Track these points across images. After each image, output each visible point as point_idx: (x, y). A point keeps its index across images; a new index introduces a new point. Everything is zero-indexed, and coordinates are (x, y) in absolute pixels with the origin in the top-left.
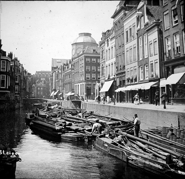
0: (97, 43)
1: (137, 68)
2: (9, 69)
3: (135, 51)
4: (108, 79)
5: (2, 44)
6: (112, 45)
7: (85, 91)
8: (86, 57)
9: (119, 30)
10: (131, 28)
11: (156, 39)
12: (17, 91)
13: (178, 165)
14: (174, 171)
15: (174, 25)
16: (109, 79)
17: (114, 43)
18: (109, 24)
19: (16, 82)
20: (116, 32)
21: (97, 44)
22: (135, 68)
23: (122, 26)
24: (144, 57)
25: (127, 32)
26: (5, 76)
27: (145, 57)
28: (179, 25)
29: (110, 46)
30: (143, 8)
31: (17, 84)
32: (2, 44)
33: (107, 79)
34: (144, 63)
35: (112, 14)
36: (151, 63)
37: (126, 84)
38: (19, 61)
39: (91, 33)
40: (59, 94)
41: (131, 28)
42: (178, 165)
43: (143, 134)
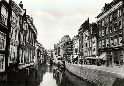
16: (76, 54)
18: (77, 33)
20: (79, 37)
32: (92, 23)
33: (75, 54)
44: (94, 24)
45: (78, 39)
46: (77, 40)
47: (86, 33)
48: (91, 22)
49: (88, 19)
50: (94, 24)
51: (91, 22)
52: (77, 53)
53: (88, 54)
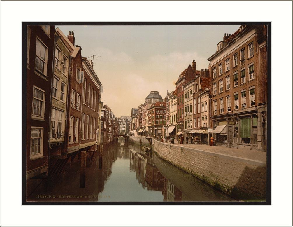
1: (192, 119)
3: (102, 124)
4: (172, 125)
6: (175, 102)
8: (156, 109)
10: (186, 94)
12: (110, 131)
14: (239, 200)
15: (235, 86)
16: (172, 125)
18: (173, 88)
19: (110, 125)
20: (177, 94)
22: (191, 119)
23: (183, 90)
25: (186, 94)
26: (80, 69)
29: (173, 103)
31: (110, 126)
34: (197, 116)
35: (176, 81)
37: (184, 129)
38: (110, 110)
39: (132, 109)
41: (186, 94)
44: (204, 71)
45: (174, 99)
46: (173, 101)
47: (191, 88)
49: (194, 62)
50: (204, 71)
52: (174, 124)
53: (195, 126)
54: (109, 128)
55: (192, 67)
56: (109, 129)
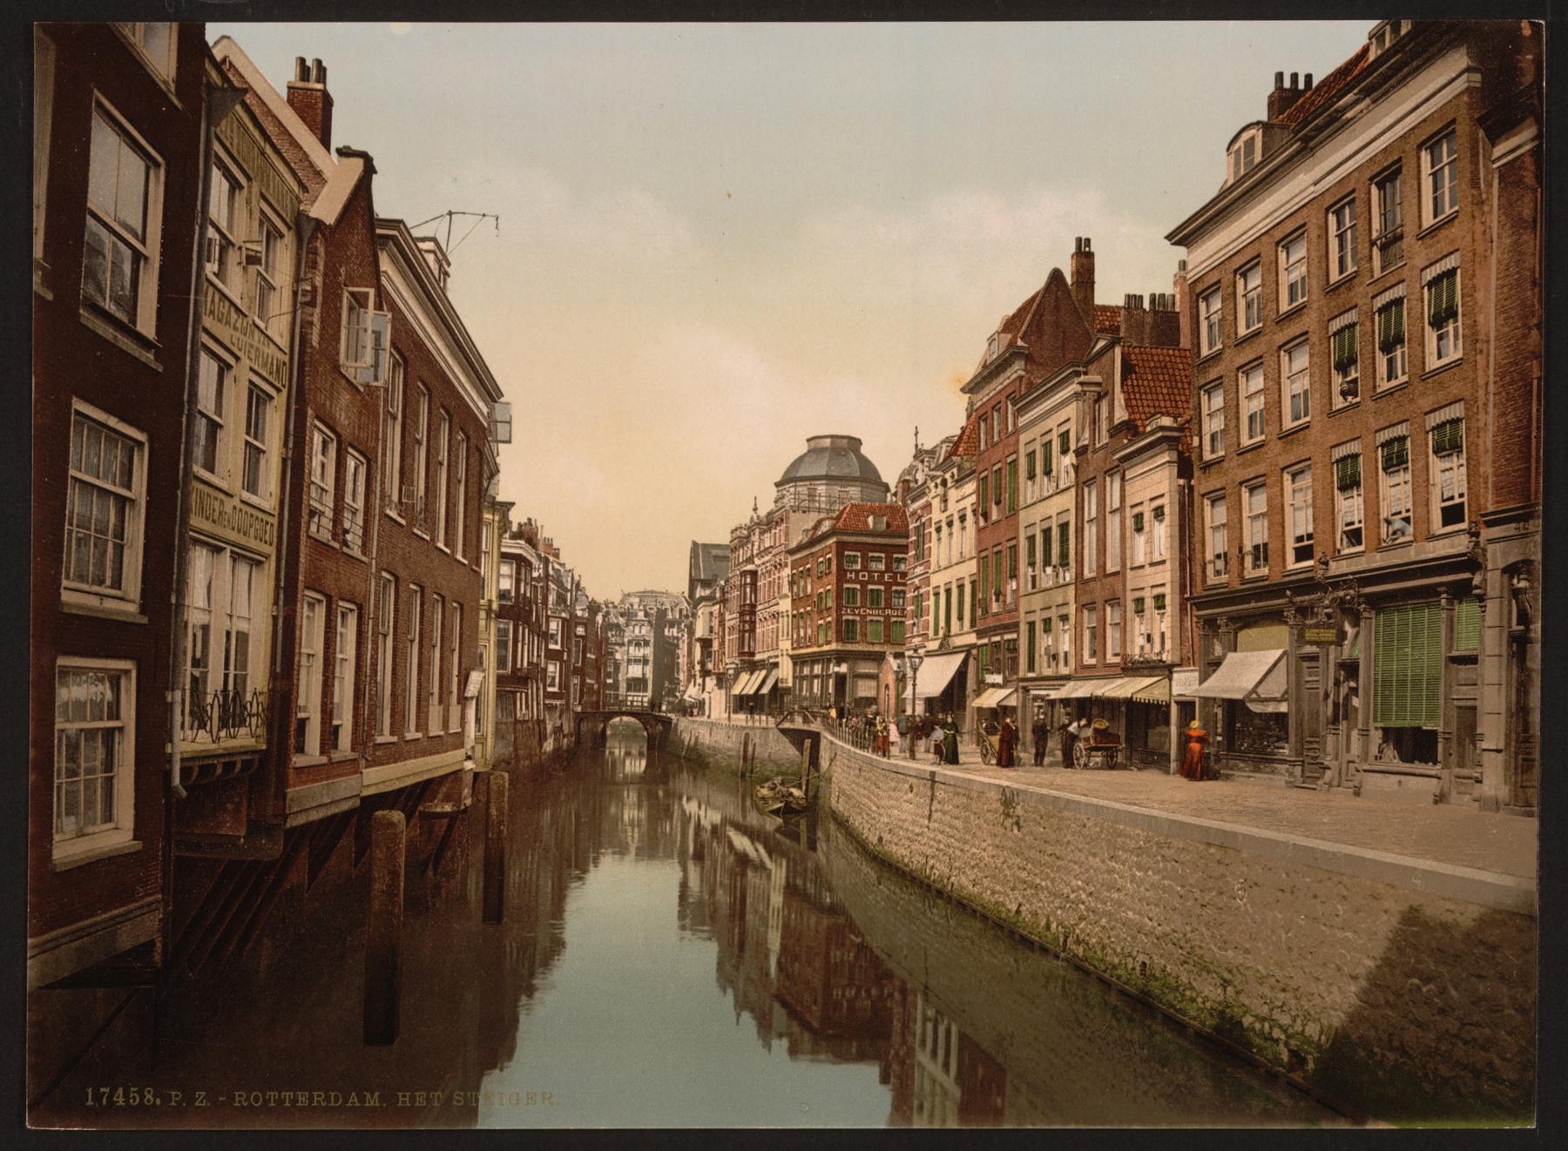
0: (884, 479)
1: (1072, 609)
2: (691, 693)
4: (941, 646)
5: (1121, 302)
7: (1331, 154)
9: (994, 445)
10: (1034, 452)
11: (1162, 496)
13: (120, 180)
16: (945, 650)
17: (973, 498)
18: (947, 417)
21: (886, 487)
22: (1063, 611)
24: (1102, 566)
27: (1110, 569)
28: (1225, 464)
30: (1109, 354)
32: (1121, 302)
33: (933, 645)
34: (1099, 593)
35: (970, 370)
36: (1138, 594)
40: (978, 693)
41: (1034, 452)
42: (120, 180)
43: (135, 235)
44: (1146, 305)
46: (953, 494)
47: (1061, 413)
48: (1109, 292)
49: (1084, 255)
50: (1146, 305)
51: (1109, 292)
54: (551, 668)
55: (1069, 280)
56: (545, 670)
